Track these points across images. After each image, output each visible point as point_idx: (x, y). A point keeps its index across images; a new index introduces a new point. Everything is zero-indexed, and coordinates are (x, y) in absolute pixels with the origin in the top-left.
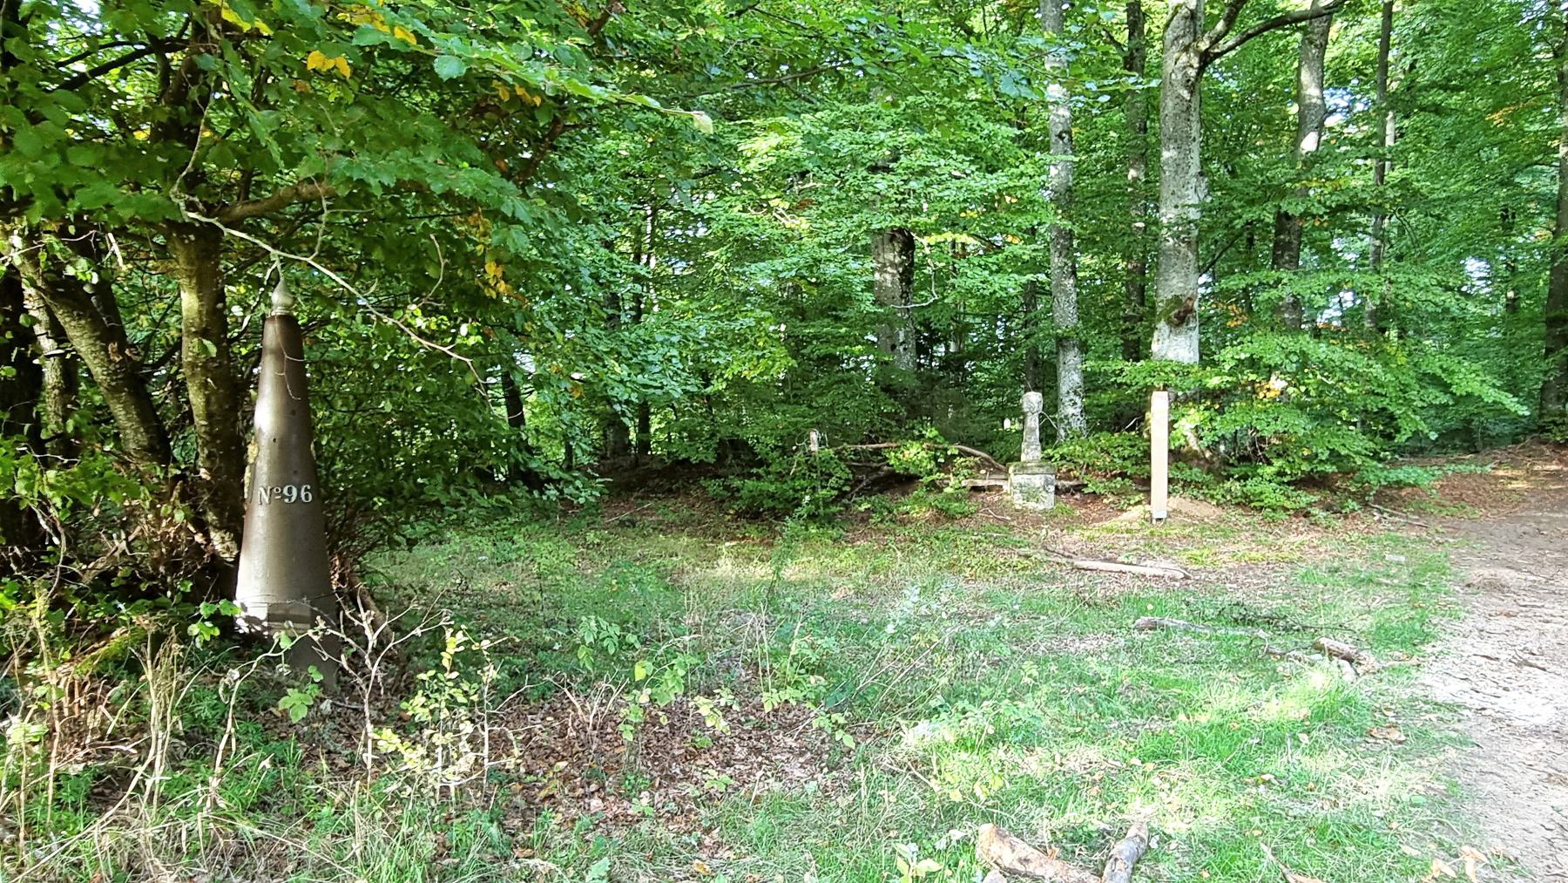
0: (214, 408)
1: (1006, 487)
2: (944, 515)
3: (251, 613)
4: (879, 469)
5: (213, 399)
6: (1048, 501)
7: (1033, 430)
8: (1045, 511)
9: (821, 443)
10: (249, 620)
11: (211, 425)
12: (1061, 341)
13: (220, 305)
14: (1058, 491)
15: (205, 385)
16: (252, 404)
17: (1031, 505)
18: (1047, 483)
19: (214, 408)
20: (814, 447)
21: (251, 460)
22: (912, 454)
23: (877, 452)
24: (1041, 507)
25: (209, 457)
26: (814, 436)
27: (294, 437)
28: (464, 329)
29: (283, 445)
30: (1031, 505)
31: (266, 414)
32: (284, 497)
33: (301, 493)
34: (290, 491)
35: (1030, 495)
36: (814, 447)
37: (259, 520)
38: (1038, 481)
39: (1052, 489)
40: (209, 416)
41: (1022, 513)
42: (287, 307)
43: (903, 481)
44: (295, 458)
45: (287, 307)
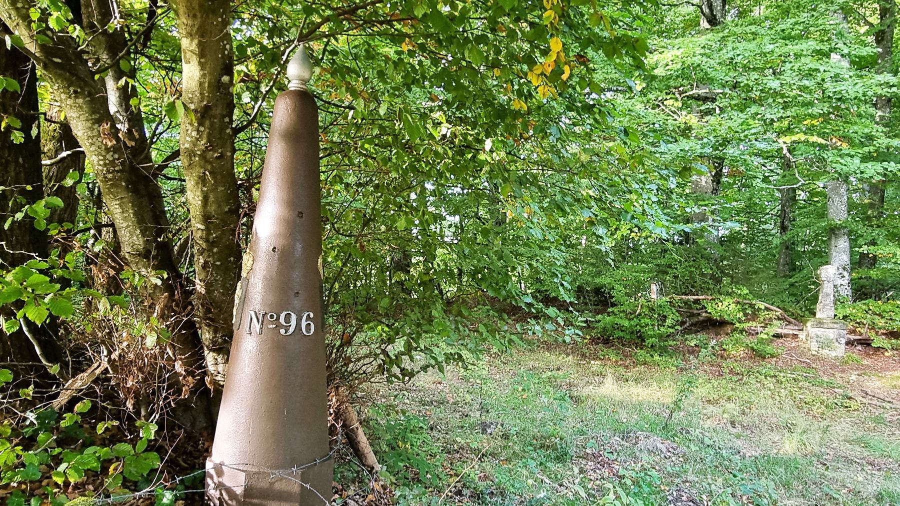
0: (212, 209)
1: (802, 336)
2: (757, 355)
3: (227, 481)
4: (699, 314)
5: (212, 198)
6: (840, 350)
7: (828, 295)
8: (836, 358)
9: (660, 292)
10: (220, 486)
11: (208, 230)
12: (833, 231)
13: (225, 79)
14: (849, 343)
15: (202, 180)
16: (253, 208)
17: (825, 352)
18: (840, 336)
19: (212, 209)
20: (654, 296)
21: (244, 274)
22: (725, 307)
23: (696, 302)
24: (834, 354)
25: (205, 267)
26: (654, 288)
27: (299, 246)
28: (488, 144)
29: (284, 257)
30: (825, 352)
31: (269, 219)
32: (279, 326)
33: (302, 323)
34: (288, 318)
35: (826, 344)
36: (654, 296)
37: (249, 346)
38: (831, 334)
39: (843, 341)
40: (206, 218)
41: (817, 358)
42: (305, 82)
43: (716, 325)
44: (297, 275)
45: (305, 82)
